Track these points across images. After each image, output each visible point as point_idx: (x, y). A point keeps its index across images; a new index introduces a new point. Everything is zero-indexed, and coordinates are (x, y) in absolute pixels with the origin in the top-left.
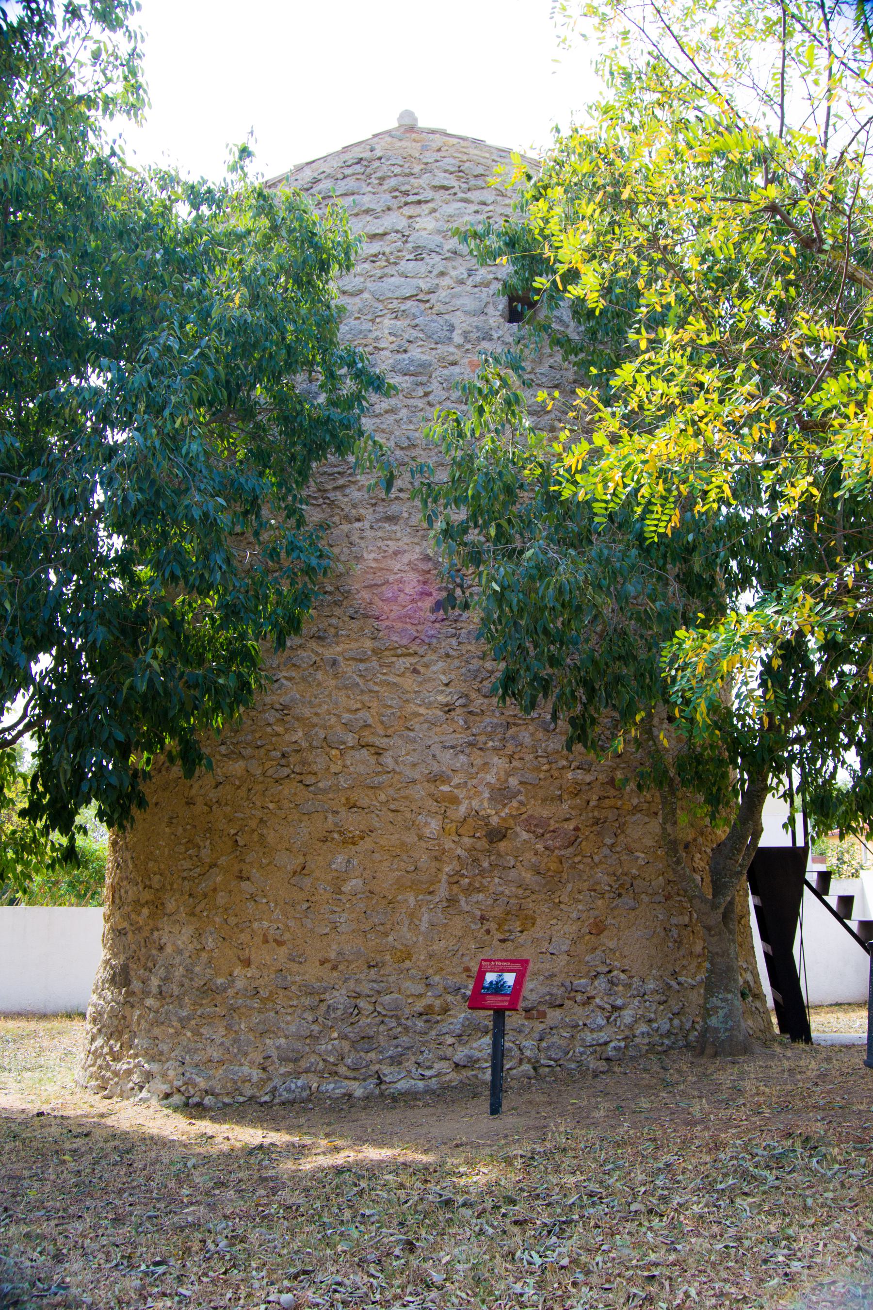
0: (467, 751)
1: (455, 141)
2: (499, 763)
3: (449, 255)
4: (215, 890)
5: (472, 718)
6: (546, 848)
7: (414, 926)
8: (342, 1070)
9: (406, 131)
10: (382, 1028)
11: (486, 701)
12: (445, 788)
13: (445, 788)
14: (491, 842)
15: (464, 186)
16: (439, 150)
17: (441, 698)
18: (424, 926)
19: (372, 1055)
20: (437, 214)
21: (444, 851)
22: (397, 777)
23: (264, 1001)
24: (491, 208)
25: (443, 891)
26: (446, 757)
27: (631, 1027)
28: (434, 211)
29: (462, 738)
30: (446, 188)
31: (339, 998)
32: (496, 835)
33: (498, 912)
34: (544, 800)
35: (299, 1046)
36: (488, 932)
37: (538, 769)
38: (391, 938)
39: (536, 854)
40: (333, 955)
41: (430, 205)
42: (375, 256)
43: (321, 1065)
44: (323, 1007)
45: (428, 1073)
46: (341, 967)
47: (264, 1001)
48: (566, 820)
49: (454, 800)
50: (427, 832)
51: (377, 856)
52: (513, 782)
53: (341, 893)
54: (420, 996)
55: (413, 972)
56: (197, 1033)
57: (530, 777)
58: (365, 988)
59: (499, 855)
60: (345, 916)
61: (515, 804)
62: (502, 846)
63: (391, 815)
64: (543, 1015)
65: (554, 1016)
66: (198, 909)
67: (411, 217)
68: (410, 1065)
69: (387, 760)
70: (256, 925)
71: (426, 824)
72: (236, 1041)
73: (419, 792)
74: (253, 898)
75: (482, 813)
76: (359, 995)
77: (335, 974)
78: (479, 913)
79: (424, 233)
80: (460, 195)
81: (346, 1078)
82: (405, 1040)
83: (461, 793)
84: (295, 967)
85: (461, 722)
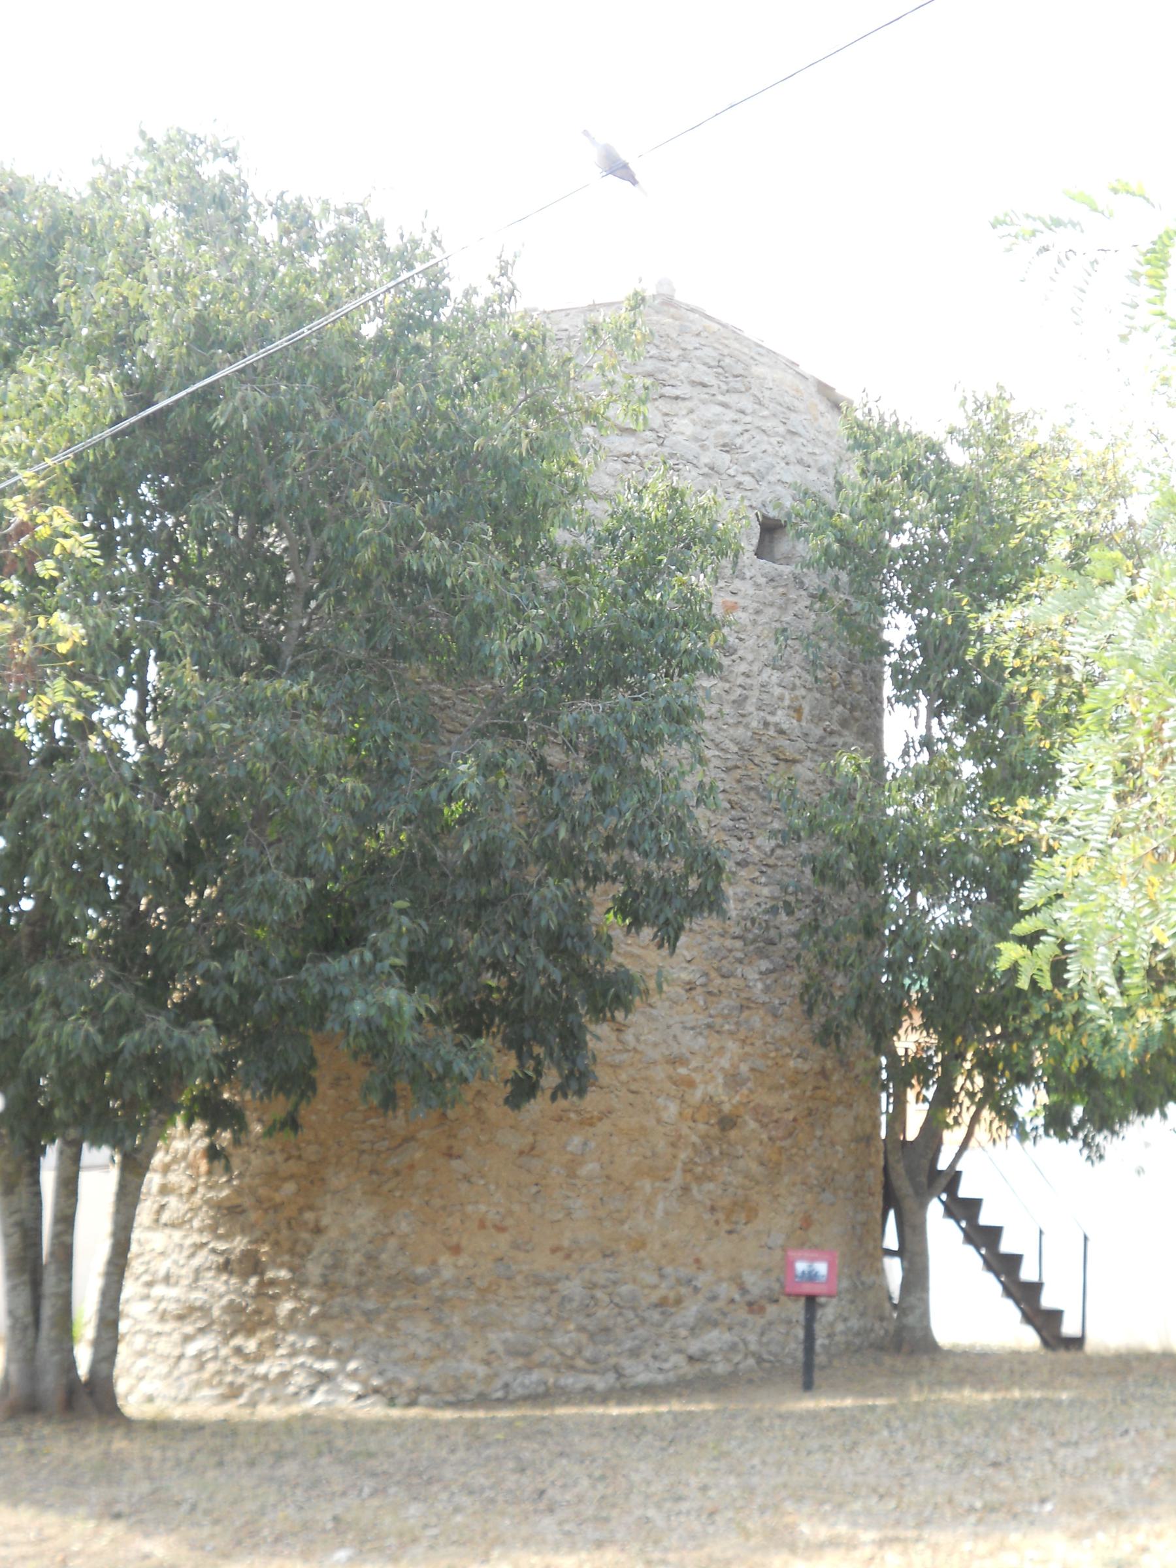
0: (706, 1032)
1: (716, 327)
2: (732, 1046)
3: (706, 470)
4: (412, 1167)
5: (710, 998)
6: (770, 1139)
7: (649, 1214)
8: (580, 1363)
9: (664, 303)
10: (620, 1320)
11: (724, 981)
12: (682, 1071)
13: (682, 1071)
14: (723, 1129)
15: (724, 387)
16: (698, 335)
17: (684, 976)
18: (659, 1213)
19: (610, 1348)
20: (693, 416)
21: (680, 1137)
22: (638, 1056)
23: (482, 1291)
24: (748, 419)
25: (677, 1178)
26: (687, 1038)
27: (832, 1325)
28: (691, 411)
29: (703, 1019)
30: (704, 386)
31: (573, 1288)
32: (727, 1123)
33: (726, 1202)
34: (770, 1089)
35: (531, 1339)
36: (717, 1222)
37: (765, 1056)
38: (626, 1227)
39: (761, 1143)
40: (566, 1243)
41: (689, 404)
42: (628, 456)
43: (558, 1359)
44: (555, 1300)
45: (666, 1366)
46: (575, 1256)
47: (482, 1291)
48: (788, 1110)
49: (691, 1084)
50: (665, 1116)
51: (615, 1140)
52: (744, 1068)
53: (575, 1176)
54: (655, 1287)
55: (647, 1262)
56: (391, 1326)
57: (760, 1063)
58: (601, 1278)
59: (729, 1144)
60: (580, 1202)
61: (745, 1091)
62: (733, 1134)
63: (631, 1096)
64: (762, 1310)
65: (772, 1310)
66: (386, 1188)
67: (667, 415)
68: (646, 1357)
69: (629, 1037)
70: (470, 1209)
71: (666, 1108)
72: (447, 1336)
73: (659, 1073)
74: (467, 1178)
75: (716, 1099)
76: (594, 1286)
77: (568, 1263)
78: (708, 1203)
79: (680, 438)
80: (720, 398)
81: (585, 1371)
82: (641, 1332)
83: (698, 1077)
84: (521, 1256)
85: (701, 1003)
